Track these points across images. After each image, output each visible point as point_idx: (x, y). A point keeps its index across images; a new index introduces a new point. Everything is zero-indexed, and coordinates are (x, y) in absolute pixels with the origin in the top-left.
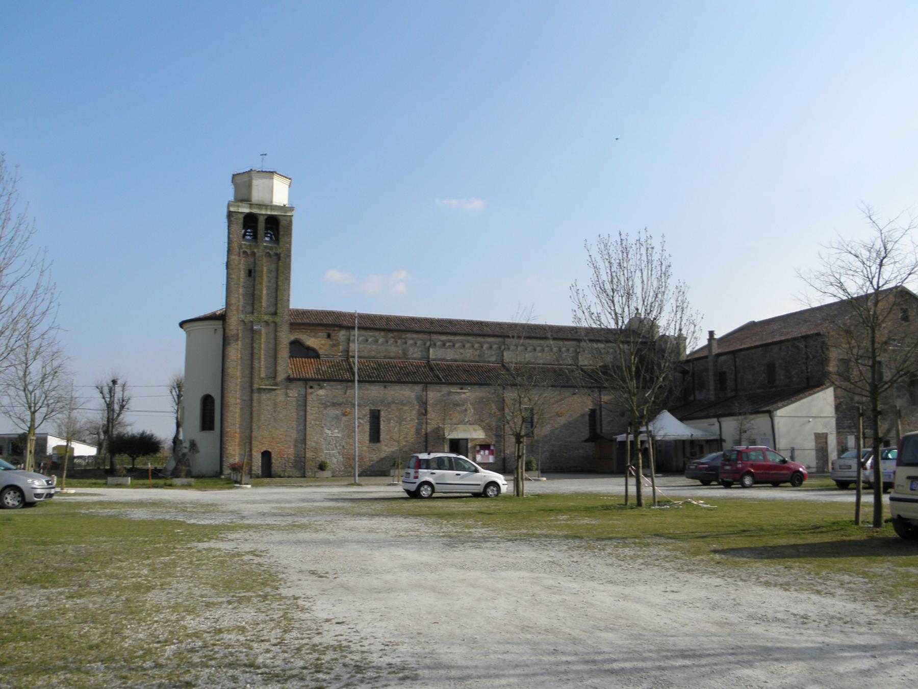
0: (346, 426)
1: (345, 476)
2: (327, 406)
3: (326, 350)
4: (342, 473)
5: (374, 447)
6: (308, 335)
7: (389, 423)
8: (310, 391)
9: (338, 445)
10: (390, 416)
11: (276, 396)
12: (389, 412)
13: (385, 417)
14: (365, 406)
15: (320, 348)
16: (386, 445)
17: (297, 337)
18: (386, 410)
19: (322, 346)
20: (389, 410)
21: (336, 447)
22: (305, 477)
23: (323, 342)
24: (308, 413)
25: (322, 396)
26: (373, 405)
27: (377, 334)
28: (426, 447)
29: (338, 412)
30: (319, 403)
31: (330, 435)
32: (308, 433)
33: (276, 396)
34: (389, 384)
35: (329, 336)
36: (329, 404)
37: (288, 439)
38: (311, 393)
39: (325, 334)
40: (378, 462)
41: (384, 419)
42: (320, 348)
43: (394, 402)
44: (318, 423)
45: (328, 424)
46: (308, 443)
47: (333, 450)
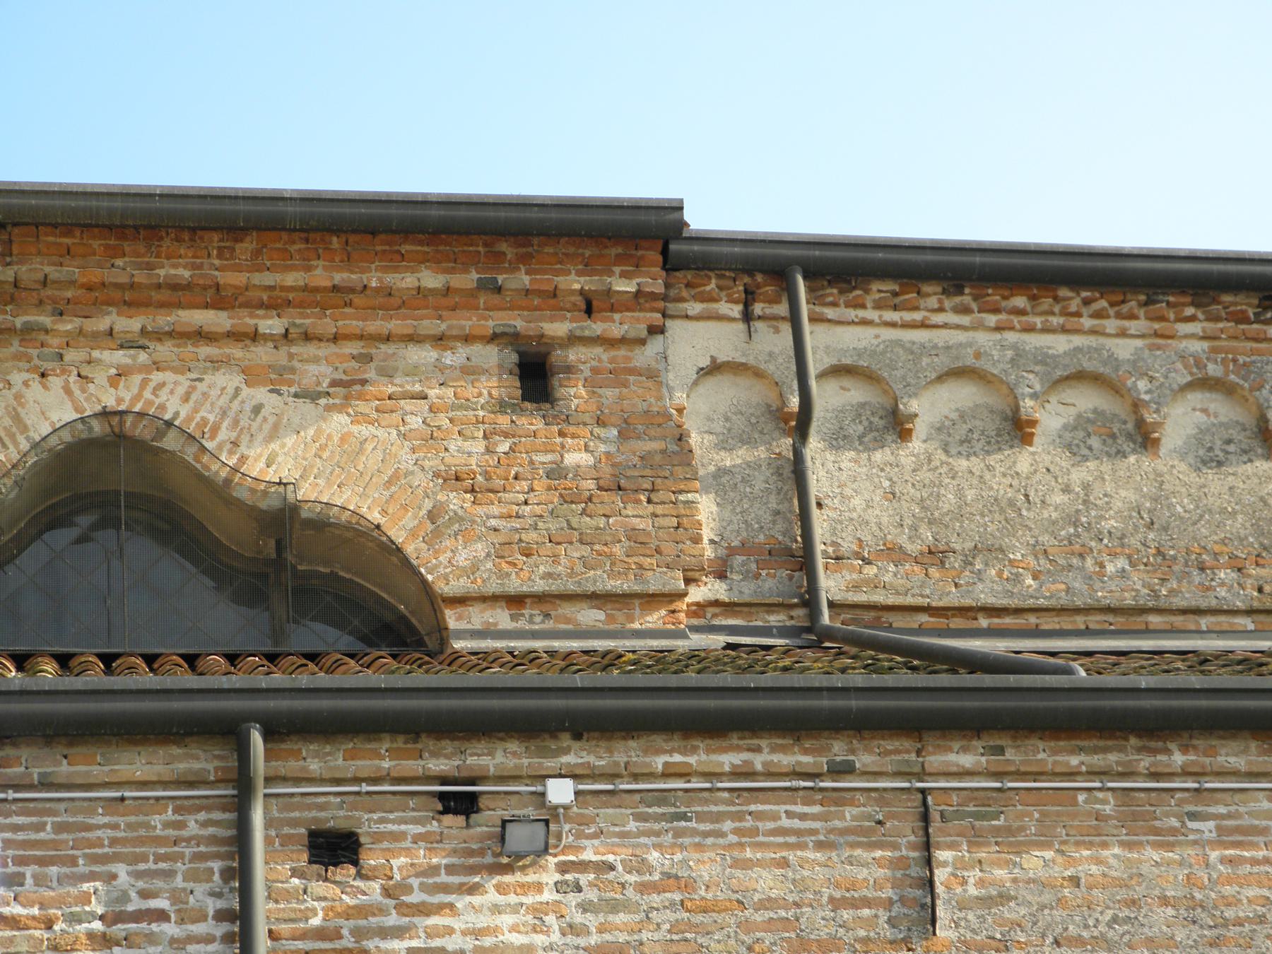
6: (252, 376)
27: (1124, 349)
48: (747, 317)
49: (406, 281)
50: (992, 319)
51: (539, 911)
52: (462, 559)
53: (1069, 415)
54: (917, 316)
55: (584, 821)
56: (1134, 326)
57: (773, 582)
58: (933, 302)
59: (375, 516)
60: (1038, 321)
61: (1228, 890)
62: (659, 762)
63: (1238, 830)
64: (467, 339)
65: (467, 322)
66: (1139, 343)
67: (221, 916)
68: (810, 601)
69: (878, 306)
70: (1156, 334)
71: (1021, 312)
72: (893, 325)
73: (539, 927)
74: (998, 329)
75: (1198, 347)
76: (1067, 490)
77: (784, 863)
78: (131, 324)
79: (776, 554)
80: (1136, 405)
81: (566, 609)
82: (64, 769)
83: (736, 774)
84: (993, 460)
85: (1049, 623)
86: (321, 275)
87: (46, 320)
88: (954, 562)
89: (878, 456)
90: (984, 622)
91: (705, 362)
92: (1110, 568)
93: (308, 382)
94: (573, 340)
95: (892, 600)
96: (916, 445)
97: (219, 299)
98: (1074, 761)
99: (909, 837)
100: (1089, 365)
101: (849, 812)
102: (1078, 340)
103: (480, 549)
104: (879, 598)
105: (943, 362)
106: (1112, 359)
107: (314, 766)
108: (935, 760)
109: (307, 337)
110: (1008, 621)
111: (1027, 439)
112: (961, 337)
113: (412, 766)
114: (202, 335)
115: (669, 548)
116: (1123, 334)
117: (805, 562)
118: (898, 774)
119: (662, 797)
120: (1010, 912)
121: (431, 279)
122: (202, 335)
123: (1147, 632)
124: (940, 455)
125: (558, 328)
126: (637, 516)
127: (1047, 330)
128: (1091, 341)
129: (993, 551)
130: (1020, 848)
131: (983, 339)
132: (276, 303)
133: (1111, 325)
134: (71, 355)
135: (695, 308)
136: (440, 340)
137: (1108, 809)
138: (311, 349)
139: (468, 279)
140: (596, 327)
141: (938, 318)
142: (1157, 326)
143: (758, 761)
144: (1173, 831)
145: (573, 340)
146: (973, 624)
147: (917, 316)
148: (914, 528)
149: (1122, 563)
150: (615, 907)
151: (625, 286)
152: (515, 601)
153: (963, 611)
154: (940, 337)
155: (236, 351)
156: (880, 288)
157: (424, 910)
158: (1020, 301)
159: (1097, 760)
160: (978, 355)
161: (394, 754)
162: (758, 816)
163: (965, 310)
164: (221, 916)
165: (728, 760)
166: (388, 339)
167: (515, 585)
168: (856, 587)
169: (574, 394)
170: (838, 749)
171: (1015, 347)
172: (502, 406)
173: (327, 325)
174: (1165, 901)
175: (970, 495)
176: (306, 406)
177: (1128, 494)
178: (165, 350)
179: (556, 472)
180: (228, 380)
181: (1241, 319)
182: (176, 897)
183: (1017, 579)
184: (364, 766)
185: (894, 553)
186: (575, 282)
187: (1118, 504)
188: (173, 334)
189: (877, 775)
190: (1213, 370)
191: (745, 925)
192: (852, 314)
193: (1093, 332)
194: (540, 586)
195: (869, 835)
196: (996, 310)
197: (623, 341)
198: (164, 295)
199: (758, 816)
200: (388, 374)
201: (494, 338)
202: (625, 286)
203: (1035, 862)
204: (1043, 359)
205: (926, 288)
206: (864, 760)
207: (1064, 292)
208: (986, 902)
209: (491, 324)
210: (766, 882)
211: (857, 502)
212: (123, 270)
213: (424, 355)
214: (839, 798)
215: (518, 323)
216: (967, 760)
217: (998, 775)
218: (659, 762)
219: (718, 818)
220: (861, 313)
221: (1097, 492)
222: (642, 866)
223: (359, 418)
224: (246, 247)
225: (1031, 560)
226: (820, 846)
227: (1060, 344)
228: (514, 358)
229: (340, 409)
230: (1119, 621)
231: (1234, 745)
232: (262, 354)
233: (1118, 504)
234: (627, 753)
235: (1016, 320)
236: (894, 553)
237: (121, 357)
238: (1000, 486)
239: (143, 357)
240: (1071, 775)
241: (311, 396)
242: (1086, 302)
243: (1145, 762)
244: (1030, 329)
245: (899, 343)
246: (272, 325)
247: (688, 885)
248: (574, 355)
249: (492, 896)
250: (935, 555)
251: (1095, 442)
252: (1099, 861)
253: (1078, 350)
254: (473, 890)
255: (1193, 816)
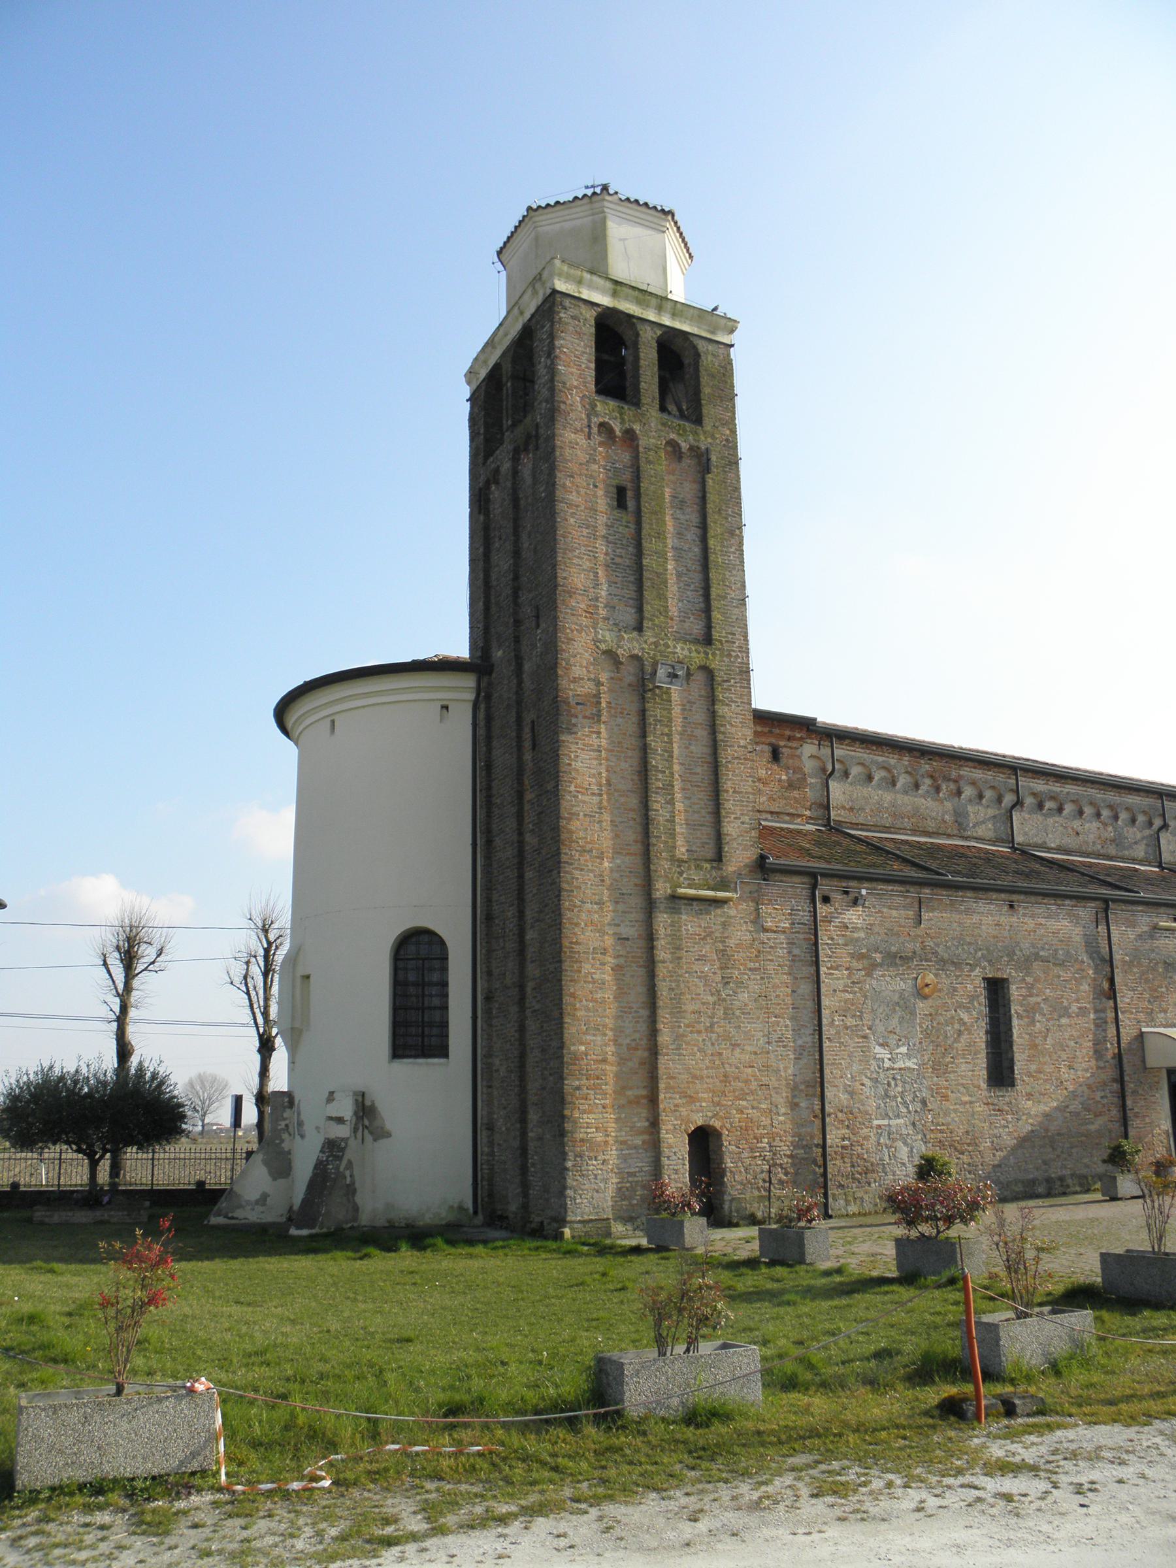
27: (892, 762)
48: (819, 745)
51: (859, 915)
57: (820, 812)
64: (763, 743)
67: (810, 911)
68: (829, 819)
73: (859, 919)
75: (907, 763)
79: (821, 805)
80: (893, 777)
81: (781, 816)
82: (784, 879)
83: (892, 891)
85: (873, 829)
88: (855, 811)
94: (785, 746)
99: (917, 906)
100: (886, 765)
103: (765, 798)
108: (923, 891)
111: (871, 782)
112: (861, 755)
113: (840, 884)
117: (827, 807)
120: (932, 922)
123: (891, 833)
125: (782, 743)
126: (796, 794)
133: (891, 755)
135: (809, 741)
139: (767, 729)
140: (790, 744)
143: (895, 888)
145: (785, 746)
150: (870, 916)
151: (798, 735)
152: (772, 813)
153: (857, 824)
154: (858, 754)
157: (840, 913)
158: (874, 748)
164: (810, 911)
165: (890, 888)
170: (908, 887)
179: (780, 780)
181: (915, 757)
182: (802, 907)
184: (832, 883)
185: (844, 808)
186: (788, 733)
190: (909, 769)
202: (798, 735)
204: (877, 763)
206: (912, 890)
209: (768, 741)
215: (774, 741)
216: (927, 891)
227: (880, 759)
234: (874, 885)
236: (844, 808)
247: (882, 913)
248: (784, 750)
250: (851, 809)
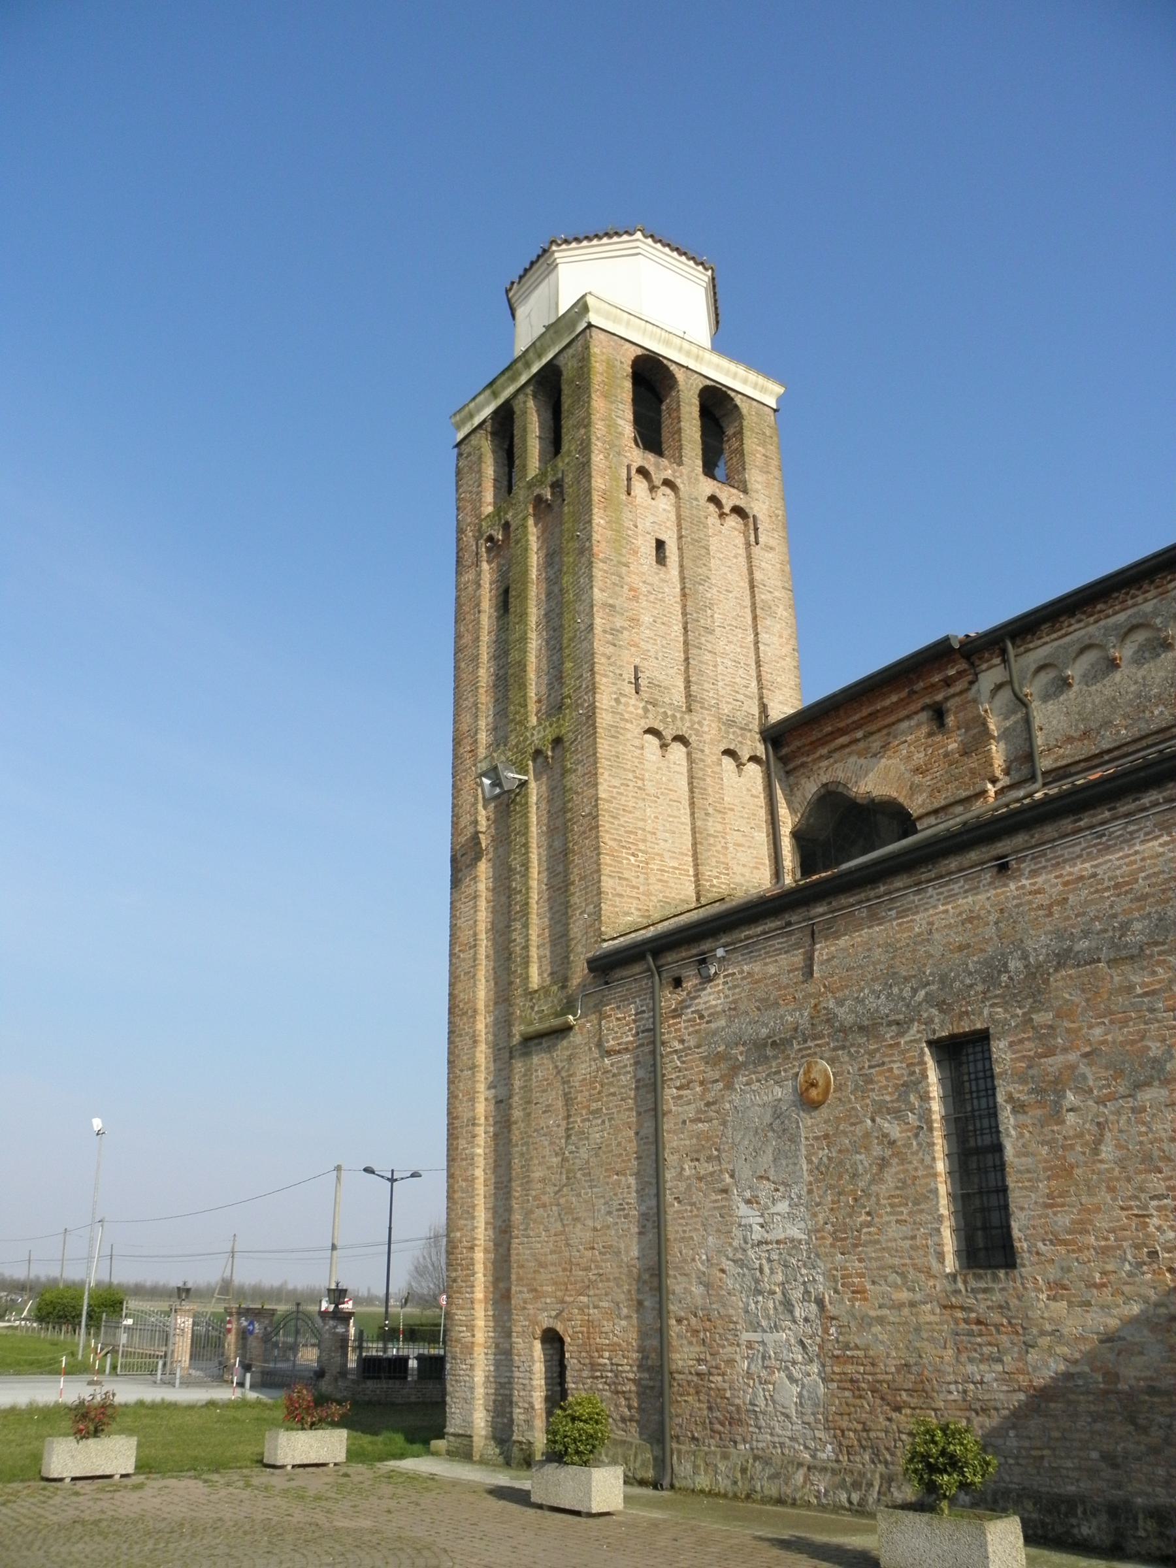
0: (820, 1171)
1: (837, 1508)
2: (735, 1069)
3: (935, 790)
4: (821, 1483)
5: (981, 1307)
6: (860, 755)
7: (1056, 1116)
8: (669, 999)
9: (796, 1295)
10: (1059, 1060)
11: (570, 1058)
12: (1044, 1036)
13: (1022, 1079)
14: (901, 1026)
15: (914, 789)
16: (1057, 1289)
17: (824, 779)
18: (1027, 1021)
19: (918, 779)
20: (1042, 1018)
21: (788, 1306)
22: (656, 1485)
23: (919, 758)
24: (668, 1124)
25: (714, 1016)
26: (942, 1006)
27: (1148, 607)
28: (437, 1403)
29: (778, 1092)
30: (706, 1060)
31: (758, 1234)
32: (673, 1230)
33: (570, 1058)
34: (1020, 839)
35: (938, 714)
36: (740, 1056)
37: (609, 1267)
38: (677, 1013)
39: (923, 716)
40: (1017, 1418)
41: (1021, 1092)
42: (914, 789)
43: (1062, 959)
44: (706, 1168)
45: (745, 1172)
46: (676, 1284)
47: (776, 1328)
49: (887, 702)
50: (1092, 619)
52: (920, 802)
53: (1135, 646)
54: (1063, 632)
55: (729, 959)
56: (1149, 595)
58: (1066, 624)
59: (895, 795)
60: (1110, 611)
61: (898, 936)
62: (743, 936)
63: (904, 911)
64: (916, 713)
65: (913, 707)
66: (1155, 601)
69: (1048, 635)
70: (1162, 594)
71: (1101, 611)
72: (1056, 639)
73: (719, 998)
74: (1096, 622)
76: (1136, 683)
77: (776, 961)
78: (824, 751)
81: (951, 810)
84: (1105, 682)
86: (865, 712)
87: (805, 759)
89: (1061, 698)
90: (1106, 758)
91: (993, 686)
92: (1156, 712)
93: (873, 750)
94: (947, 699)
95: (1070, 761)
96: (1075, 688)
97: (843, 732)
98: (851, 900)
100: (1134, 622)
101: (793, 938)
102: (1129, 612)
104: (1064, 762)
105: (1077, 647)
106: (1145, 615)
107: (670, 959)
109: (872, 734)
110: (1116, 753)
111: (1118, 666)
112: (1083, 632)
114: (843, 747)
115: (982, 772)
116: (1146, 601)
118: (804, 921)
119: (746, 947)
121: (894, 698)
122: (843, 747)
124: (1085, 688)
125: (939, 697)
127: (1115, 613)
128: (1134, 610)
129: (1107, 724)
130: (838, 938)
131: (1091, 629)
132: (858, 726)
134: (815, 768)
135: (984, 666)
136: (908, 717)
137: (864, 915)
138: (871, 739)
140: (952, 691)
141: (1071, 629)
142: (1160, 590)
144: (884, 917)
145: (947, 699)
146: (1102, 760)
147: (1063, 632)
148: (1076, 725)
149: (1161, 708)
152: (936, 812)
155: (854, 747)
156: (1045, 627)
158: (1099, 607)
159: (857, 898)
160: (1090, 638)
161: (686, 950)
162: (770, 946)
163: (1079, 621)
165: (759, 929)
166: (893, 724)
167: (936, 805)
168: (1056, 760)
169: (950, 720)
171: (1104, 627)
172: (930, 734)
173: (874, 727)
174: (879, 946)
175: (1097, 701)
176: (874, 760)
177: (1162, 674)
178: (836, 755)
180: (853, 759)
183: (1118, 732)
185: (1070, 739)
186: (936, 678)
187: (1158, 680)
188: (836, 750)
189: (800, 922)
191: (766, 985)
192: (1039, 642)
193: (1134, 605)
194: (943, 803)
195: (797, 946)
196: (1091, 615)
197: (961, 693)
198: (829, 738)
199: (770, 946)
200: (895, 737)
201: (923, 709)
203: (843, 942)
204: (1116, 627)
205: (1062, 619)
206: (794, 919)
207: (1115, 595)
208: (828, 960)
209: (920, 705)
210: (772, 969)
211: (1055, 722)
212: (816, 735)
213: (904, 725)
214: (790, 933)
215: (928, 701)
216: (820, 910)
217: (833, 912)
218: (743, 936)
219: (760, 950)
220: (1043, 640)
221: (1149, 678)
222: (741, 972)
223: (890, 758)
224: (842, 712)
225: (1124, 722)
226: (786, 952)
227: (1121, 617)
228: (931, 713)
229: (882, 757)
230: (1160, 737)
231: (899, 878)
232: (862, 745)
233: (1158, 680)
235: (1102, 615)
236: (1070, 739)
237: (826, 763)
238: (1108, 692)
239: (832, 760)
240: (853, 905)
241: (875, 755)
242: (1127, 594)
243: (872, 894)
244: (1108, 616)
245: (1060, 646)
246: (859, 734)
249: (709, 990)
250: (1086, 734)
251: (1147, 655)
252: (860, 936)
253: (1130, 616)
254: (704, 989)
255: (890, 910)
